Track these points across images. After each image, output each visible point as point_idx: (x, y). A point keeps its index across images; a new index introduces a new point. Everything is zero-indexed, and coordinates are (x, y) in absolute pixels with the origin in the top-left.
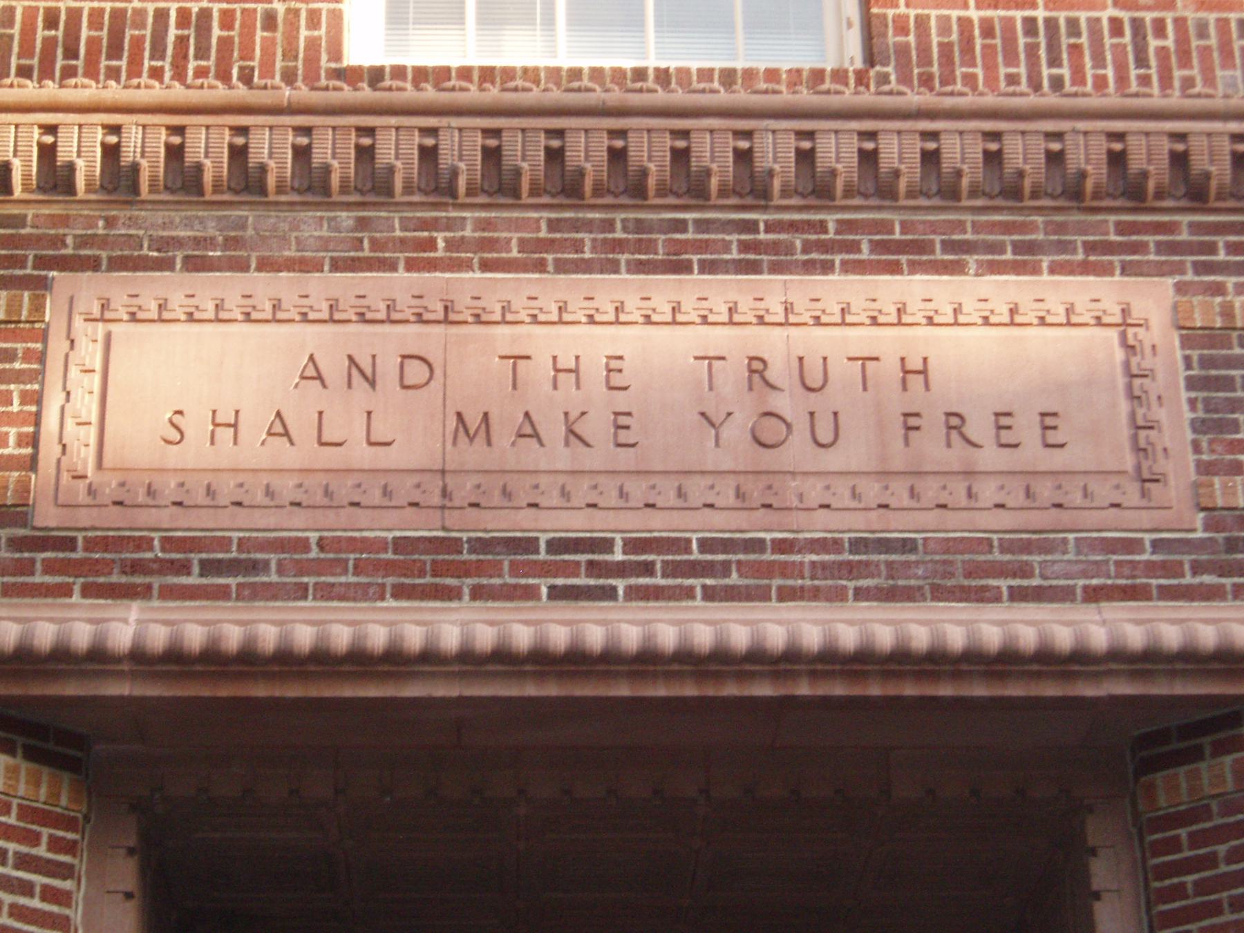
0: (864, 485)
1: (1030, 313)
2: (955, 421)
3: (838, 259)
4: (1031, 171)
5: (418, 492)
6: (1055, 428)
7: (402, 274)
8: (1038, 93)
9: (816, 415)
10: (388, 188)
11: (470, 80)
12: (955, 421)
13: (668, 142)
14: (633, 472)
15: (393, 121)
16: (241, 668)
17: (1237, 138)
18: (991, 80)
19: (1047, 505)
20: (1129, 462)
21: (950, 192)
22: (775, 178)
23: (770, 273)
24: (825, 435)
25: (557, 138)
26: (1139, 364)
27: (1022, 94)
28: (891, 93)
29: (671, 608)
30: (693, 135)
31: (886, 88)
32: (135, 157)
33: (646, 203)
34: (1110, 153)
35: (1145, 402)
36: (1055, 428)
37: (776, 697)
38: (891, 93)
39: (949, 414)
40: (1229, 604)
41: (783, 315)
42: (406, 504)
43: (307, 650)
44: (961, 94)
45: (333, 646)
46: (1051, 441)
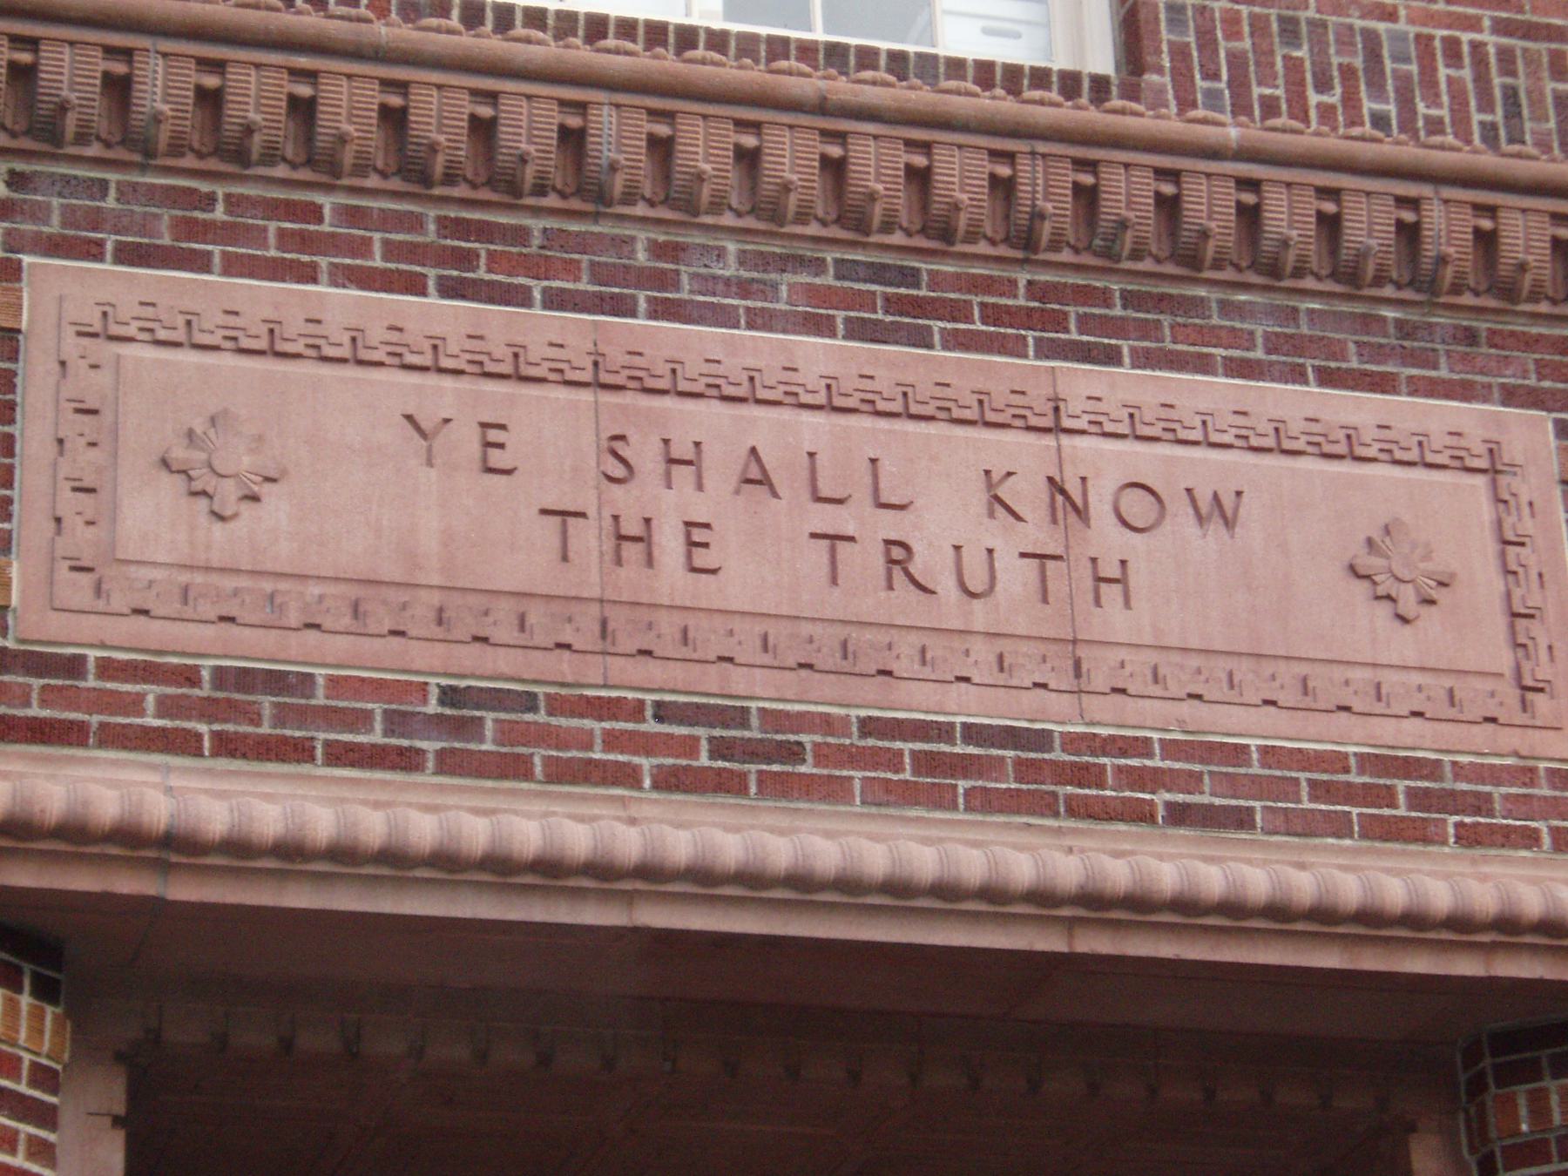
0: (1243, 669)
1: (932, 401)
2: (897, 553)
3: (323, 262)
4: (968, 202)
5: (1492, 702)
6: (706, 545)
7: (433, 300)
8: (561, 43)
9: (1100, 562)
10: (1354, 274)
11: (542, 27)
12: (897, 553)
13: (556, 117)
14: (1035, 638)
15: (436, 77)
16: (1362, 930)
17: (1558, 218)
18: (1407, 125)
19: (126, 610)
20: (1504, 660)
21: (1190, 260)
22: (69, 114)
23: (1410, 394)
24: (977, 583)
25: (1252, 191)
26: (1514, 528)
27: (450, 32)
28: (1362, 139)
29: (269, 775)
30: (1502, 214)
31: (1356, 131)
32: (1034, 199)
33: (609, 210)
34: (474, 119)
35: (1522, 582)
36: (706, 545)
37: (1553, 982)
38: (1362, 139)
39: (888, 542)
40: (960, 816)
41: (823, 392)
42: (126, 610)
43: (480, 853)
44: (1452, 149)
45: (146, 819)
46: (698, 563)
